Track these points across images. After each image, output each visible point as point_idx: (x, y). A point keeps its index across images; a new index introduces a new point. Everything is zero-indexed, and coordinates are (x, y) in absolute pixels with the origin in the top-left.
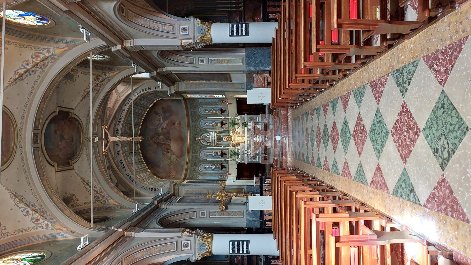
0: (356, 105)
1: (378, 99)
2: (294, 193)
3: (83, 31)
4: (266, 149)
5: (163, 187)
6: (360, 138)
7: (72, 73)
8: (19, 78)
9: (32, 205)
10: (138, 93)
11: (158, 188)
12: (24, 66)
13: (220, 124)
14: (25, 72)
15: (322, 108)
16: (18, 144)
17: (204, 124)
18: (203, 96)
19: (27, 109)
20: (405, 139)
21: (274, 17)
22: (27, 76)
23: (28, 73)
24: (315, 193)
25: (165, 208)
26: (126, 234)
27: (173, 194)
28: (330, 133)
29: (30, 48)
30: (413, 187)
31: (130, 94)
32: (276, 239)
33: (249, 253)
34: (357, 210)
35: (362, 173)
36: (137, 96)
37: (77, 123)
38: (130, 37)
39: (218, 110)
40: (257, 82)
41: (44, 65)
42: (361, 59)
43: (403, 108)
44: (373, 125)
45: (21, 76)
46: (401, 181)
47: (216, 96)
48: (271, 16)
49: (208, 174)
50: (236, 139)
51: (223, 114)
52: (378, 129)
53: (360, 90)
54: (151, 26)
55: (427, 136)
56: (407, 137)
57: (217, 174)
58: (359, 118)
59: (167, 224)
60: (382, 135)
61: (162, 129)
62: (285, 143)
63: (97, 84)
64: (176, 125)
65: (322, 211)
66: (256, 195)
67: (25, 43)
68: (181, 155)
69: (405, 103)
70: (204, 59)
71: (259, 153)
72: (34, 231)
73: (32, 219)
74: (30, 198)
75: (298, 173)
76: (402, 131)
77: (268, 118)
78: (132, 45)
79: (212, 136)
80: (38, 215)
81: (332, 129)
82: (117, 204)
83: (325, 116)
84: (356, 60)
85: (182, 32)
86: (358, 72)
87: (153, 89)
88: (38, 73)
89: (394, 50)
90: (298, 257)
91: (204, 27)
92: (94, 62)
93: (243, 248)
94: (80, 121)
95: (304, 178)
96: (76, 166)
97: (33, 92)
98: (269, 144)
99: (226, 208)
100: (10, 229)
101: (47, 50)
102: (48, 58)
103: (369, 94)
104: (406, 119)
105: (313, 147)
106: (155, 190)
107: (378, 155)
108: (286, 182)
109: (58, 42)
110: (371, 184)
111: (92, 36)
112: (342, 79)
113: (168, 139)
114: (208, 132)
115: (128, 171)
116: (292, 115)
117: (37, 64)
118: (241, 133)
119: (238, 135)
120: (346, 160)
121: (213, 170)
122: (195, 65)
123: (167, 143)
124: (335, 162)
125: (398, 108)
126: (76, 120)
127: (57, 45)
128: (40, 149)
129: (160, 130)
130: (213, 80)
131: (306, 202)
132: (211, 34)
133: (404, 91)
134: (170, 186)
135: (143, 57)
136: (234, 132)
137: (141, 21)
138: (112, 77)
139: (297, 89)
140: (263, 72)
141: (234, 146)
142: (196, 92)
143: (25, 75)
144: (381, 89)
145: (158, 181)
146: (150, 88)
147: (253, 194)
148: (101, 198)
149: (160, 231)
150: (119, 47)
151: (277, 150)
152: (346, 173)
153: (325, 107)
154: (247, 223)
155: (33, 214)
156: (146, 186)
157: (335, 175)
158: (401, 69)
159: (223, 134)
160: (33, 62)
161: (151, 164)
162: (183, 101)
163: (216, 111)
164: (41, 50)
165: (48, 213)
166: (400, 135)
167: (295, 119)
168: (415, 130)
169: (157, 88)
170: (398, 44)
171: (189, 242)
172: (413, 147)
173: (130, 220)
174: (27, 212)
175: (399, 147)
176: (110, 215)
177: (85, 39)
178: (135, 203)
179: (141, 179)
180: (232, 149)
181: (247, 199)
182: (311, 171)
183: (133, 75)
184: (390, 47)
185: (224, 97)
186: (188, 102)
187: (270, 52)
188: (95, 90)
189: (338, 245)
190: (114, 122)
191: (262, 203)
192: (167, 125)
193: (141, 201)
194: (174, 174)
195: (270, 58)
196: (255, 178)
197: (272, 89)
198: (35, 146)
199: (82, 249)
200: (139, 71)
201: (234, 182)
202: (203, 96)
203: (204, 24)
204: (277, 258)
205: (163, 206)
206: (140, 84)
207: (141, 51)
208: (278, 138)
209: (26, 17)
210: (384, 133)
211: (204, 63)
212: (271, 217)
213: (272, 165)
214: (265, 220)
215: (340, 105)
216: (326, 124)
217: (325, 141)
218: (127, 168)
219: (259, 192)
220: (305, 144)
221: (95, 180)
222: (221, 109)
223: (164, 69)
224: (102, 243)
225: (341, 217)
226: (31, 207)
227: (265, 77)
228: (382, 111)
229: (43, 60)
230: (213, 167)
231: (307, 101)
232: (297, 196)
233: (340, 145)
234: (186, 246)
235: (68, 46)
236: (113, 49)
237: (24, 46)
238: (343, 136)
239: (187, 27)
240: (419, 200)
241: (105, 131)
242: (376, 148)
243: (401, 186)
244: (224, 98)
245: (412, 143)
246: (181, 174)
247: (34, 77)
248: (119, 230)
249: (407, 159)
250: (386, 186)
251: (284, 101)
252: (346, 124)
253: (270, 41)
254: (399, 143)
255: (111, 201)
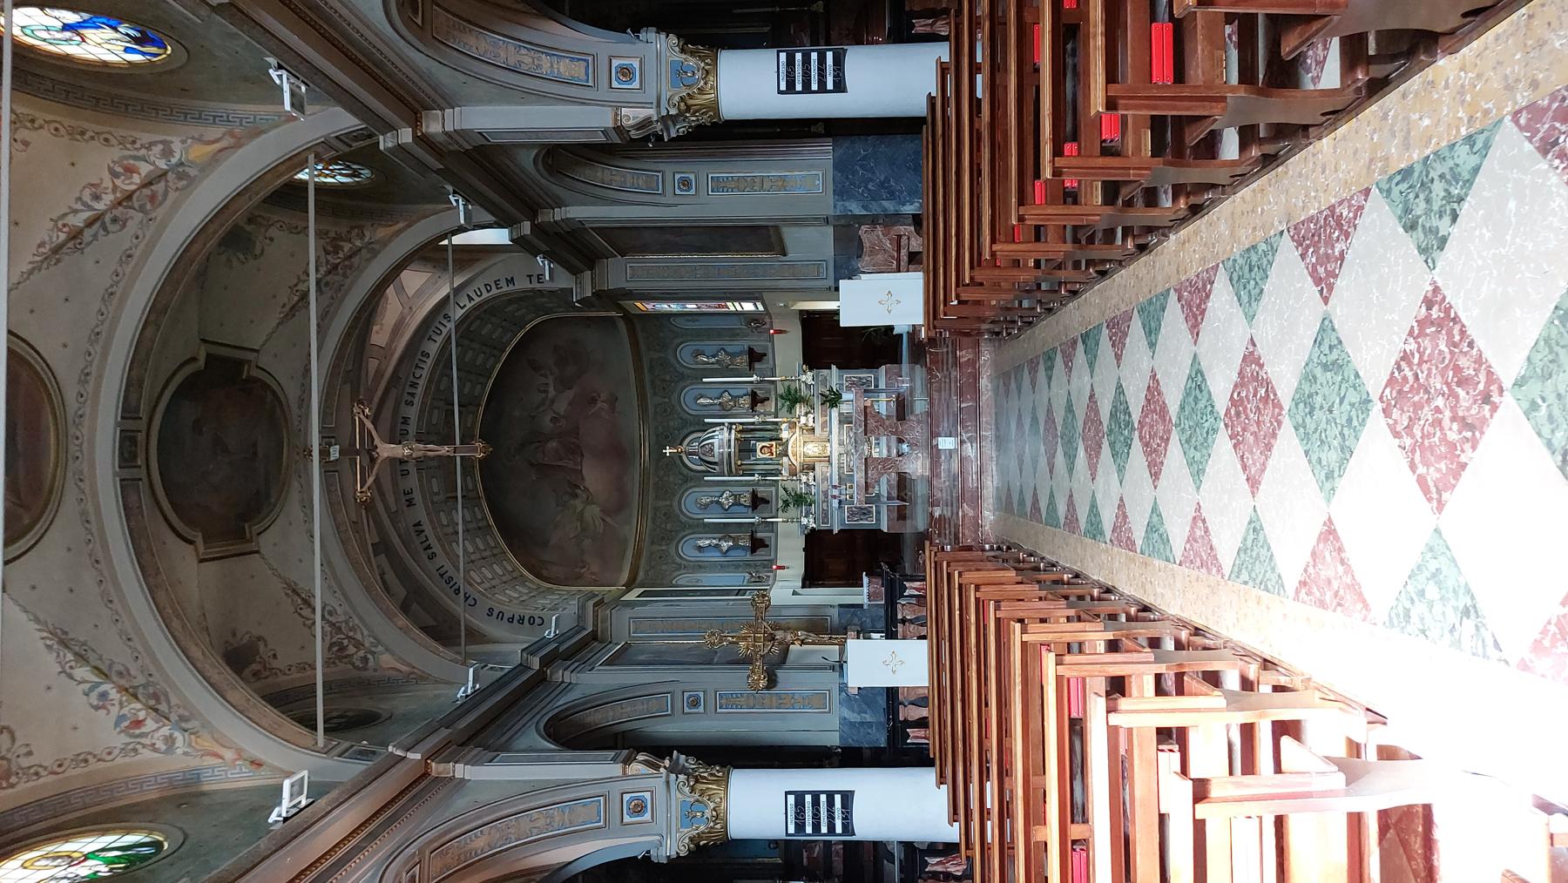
0: (1237, 311)
1: (1325, 284)
2: (1052, 656)
3: (280, 77)
4: (903, 482)
5: (559, 611)
6: (1254, 428)
7: (249, 228)
8: (70, 245)
9: (120, 674)
10: (471, 299)
11: (541, 614)
12: (85, 204)
13: (745, 402)
14: (90, 224)
15: (1105, 332)
16: (72, 466)
17: (696, 399)
18: (691, 307)
19: (98, 348)
20: (1438, 423)
21: (928, 29)
22: (95, 236)
23: (98, 224)
24: (1088, 626)
25: (567, 680)
26: (436, 768)
27: (594, 636)
28: (1136, 417)
29: (106, 140)
30: (1473, 598)
31: (446, 299)
32: (944, 787)
33: (853, 834)
34: (1247, 685)
35: (1264, 552)
36: (469, 305)
37: (269, 397)
38: (440, 101)
39: (740, 354)
40: (873, 252)
41: (152, 198)
42: (1261, 142)
43: (1429, 308)
44: (1306, 378)
45: (76, 235)
46: (1422, 578)
47: (732, 307)
48: (920, 26)
49: (707, 568)
50: (800, 450)
51: (757, 365)
52: (1326, 390)
53: (1254, 258)
54: (512, 62)
55: (1534, 406)
56: (1448, 414)
57: (737, 567)
58: (1251, 358)
59: (575, 735)
60: (1341, 413)
61: (554, 420)
62: (971, 464)
63: (335, 267)
64: (599, 405)
65: (1117, 687)
66: (873, 635)
67: (86, 125)
68: (617, 507)
69: (1436, 290)
70: (692, 177)
71: (878, 495)
72: (127, 759)
73: (121, 718)
74: (114, 650)
75: (1019, 561)
76: (1427, 391)
77: (909, 378)
78: (449, 128)
79: (721, 440)
80: (139, 706)
81: (1143, 402)
82: (404, 668)
83: (1118, 357)
84: (1243, 146)
85: (618, 79)
86: (1245, 192)
87: (522, 284)
88: (132, 226)
89: (1391, 101)
90: (1037, 852)
91: (692, 62)
92: (321, 189)
93: (831, 817)
94: (280, 394)
95: (1042, 576)
96: (267, 541)
97: (119, 290)
98: (917, 466)
99: (772, 682)
100: (44, 755)
101: (160, 147)
102: (165, 174)
103: (1289, 268)
104: (1443, 347)
105: (1071, 470)
106: (532, 620)
107: (1328, 485)
108: (983, 589)
109: (200, 118)
110: (1297, 592)
111: (315, 100)
112: (1183, 221)
113: (575, 451)
114: (705, 428)
115: (441, 560)
116: (996, 364)
117: (129, 197)
118: (818, 430)
119: (808, 437)
120: (1199, 508)
121: (725, 554)
122: (662, 200)
123: (570, 465)
124: (1155, 519)
125: (1410, 309)
126: (265, 386)
127: (195, 131)
128: (143, 486)
129: (546, 422)
130: (725, 249)
131: (1061, 660)
132: (715, 88)
133: (1433, 246)
134: (582, 607)
135: (488, 172)
136: (792, 426)
137: (482, 44)
138: (385, 243)
139: (1016, 263)
140: (896, 218)
141: (793, 473)
142: (668, 293)
143: (88, 235)
144: (1338, 247)
145: (543, 593)
146: (511, 281)
147: (864, 633)
148: (352, 650)
149: (548, 760)
150: (406, 135)
151: (943, 481)
152: (1197, 554)
153: (1118, 328)
154: (841, 731)
155: (121, 703)
156: (503, 608)
157: (1156, 562)
158: (1418, 168)
159: (758, 434)
160: (115, 188)
161: (522, 539)
162: (622, 326)
163: (733, 355)
164: (142, 146)
165: (174, 701)
166: (1418, 407)
167: (1007, 378)
168: (1481, 387)
169: (534, 279)
170: (1405, 76)
171: (647, 795)
172: (1474, 448)
173: (448, 722)
174: (104, 695)
175: (1413, 451)
176: (383, 707)
177: (288, 107)
178: (464, 663)
179: (487, 585)
180: (789, 485)
181: (842, 652)
182: (1070, 554)
183: (454, 233)
184: (1377, 87)
185: (761, 308)
186: (638, 327)
187: (917, 153)
188: (327, 284)
189: (1203, 810)
190: (394, 392)
191: (894, 663)
192: (570, 404)
193: (484, 660)
194: (595, 568)
195: (917, 169)
196: (865, 580)
197: (927, 273)
198: (127, 473)
199: (286, 819)
200: (475, 221)
201: (795, 593)
202: (691, 307)
203: (692, 53)
204: (949, 849)
205: (560, 675)
206: (478, 268)
207: (480, 149)
208: (946, 443)
209: (88, 33)
210: (1352, 405)
211: (693, 192)
212: (924, 712)
213: (922, 538)
214: (906, 720)
215: (1174, 315)
216: (1119, 386)
217: (1118, 446)
218: (437, 548)
219: (881, 624)
220: (1043, 461)
221: (330, 587)
222: (751, 351)
223: (559, 214)
224: (353, 800)
225: (1198, 710)
226: (115, 678)
227: (900, 237)
228: (1344, 328)
229: (150, 183)
230: (725, 545)
231: (1050, 310)
232: (1026, 638)
233: (1174, 456)
234: (639, 809)
235: (232, 134)
236: (385, 142)
237: (83, 133)
238: (1186, 424)
239: (636, 64)
240: (1497, 646)
241: (362, 424)
242: (1320, 461)
243: (1422, 593)
244: (760, 314)
245: (1469, 434)
246: (620, 570)
247: (121, 239)
248: (411, 756)
249: (1445, 496)
250: (1360, 594)
251: (966, 311)
252: (1197, 381)
253: (919, 108)
254: (1413, 436)
255: (386, 660)
